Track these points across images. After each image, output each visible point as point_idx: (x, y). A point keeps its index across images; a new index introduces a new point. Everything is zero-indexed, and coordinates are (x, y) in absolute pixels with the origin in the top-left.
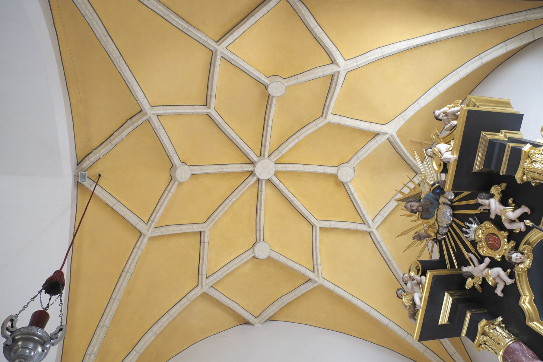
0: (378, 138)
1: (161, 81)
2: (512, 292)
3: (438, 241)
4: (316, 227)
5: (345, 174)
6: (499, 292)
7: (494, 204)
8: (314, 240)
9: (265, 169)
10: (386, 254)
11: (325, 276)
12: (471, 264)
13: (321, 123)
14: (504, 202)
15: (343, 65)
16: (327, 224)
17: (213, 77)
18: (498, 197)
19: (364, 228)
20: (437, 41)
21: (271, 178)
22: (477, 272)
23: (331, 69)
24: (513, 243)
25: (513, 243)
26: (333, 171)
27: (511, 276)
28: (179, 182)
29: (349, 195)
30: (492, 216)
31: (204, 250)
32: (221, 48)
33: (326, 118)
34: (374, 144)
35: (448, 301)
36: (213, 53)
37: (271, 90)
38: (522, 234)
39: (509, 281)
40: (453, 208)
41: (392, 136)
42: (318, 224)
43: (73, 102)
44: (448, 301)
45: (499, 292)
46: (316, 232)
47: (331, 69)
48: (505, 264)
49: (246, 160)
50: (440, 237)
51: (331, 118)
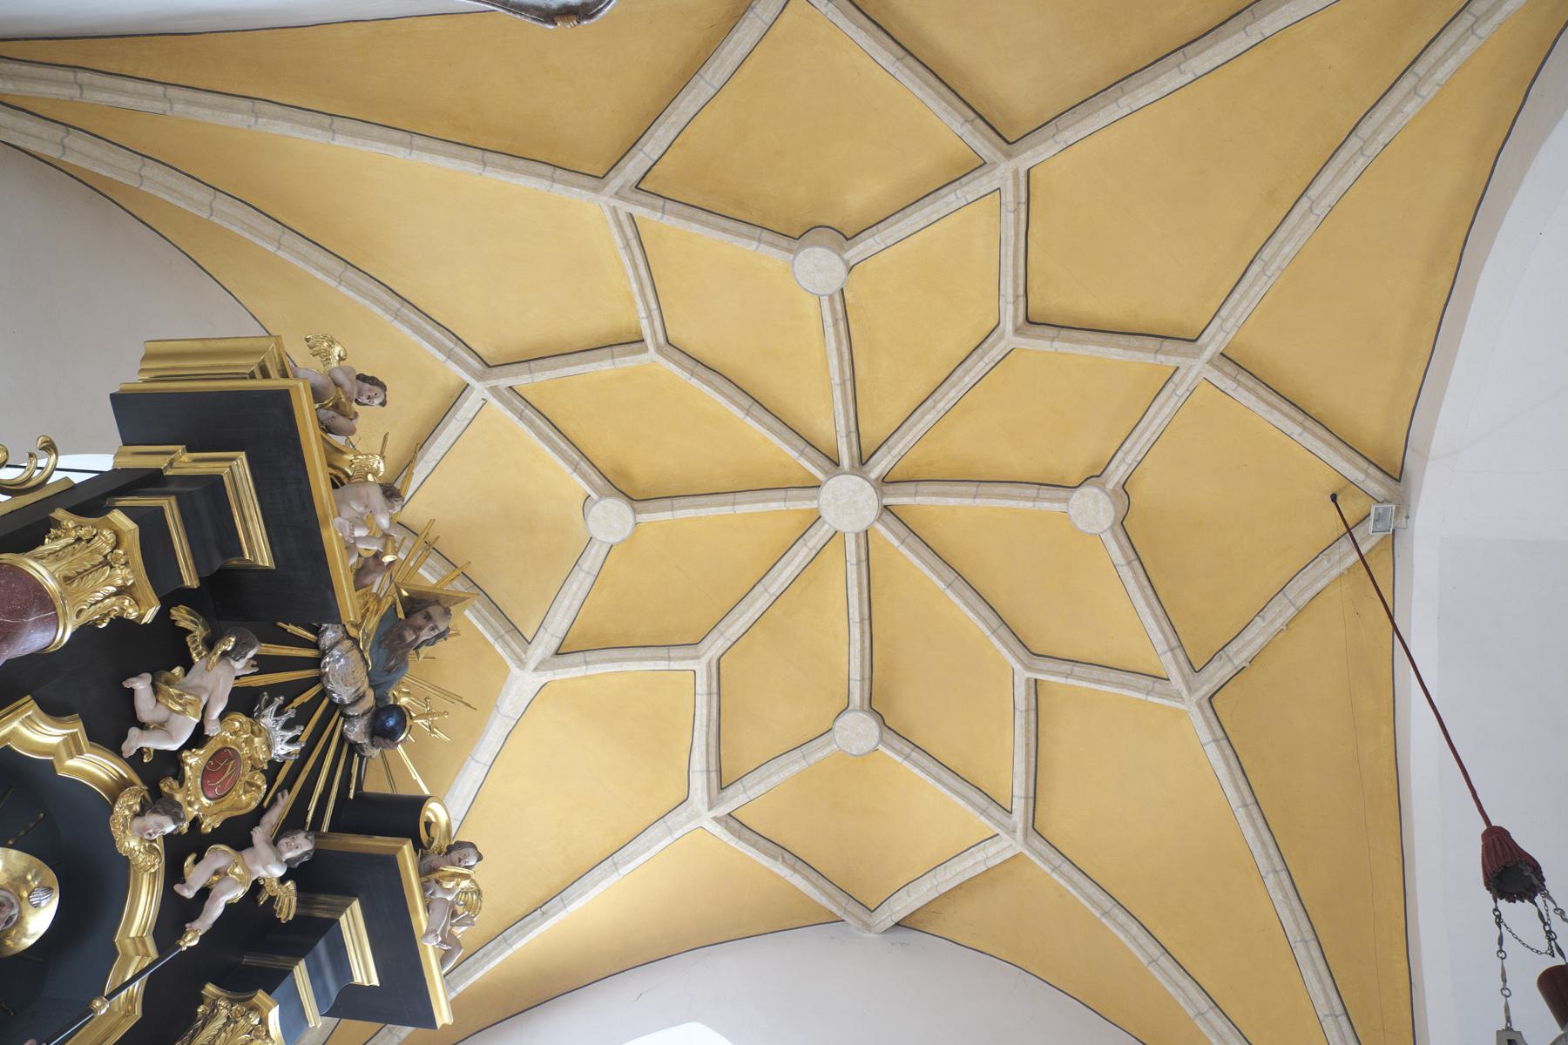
1: (1157, 768)
4: (659, 350)
5: (611, 520)
6: (141, 686)
7: (268, 866)
8: (653, 306)
9: (848, 502)
10: (417, 330)
11: (592, 211)
13: (715, 646)
15: (701, 821)
16: (628, 362)
17: (1027, 762)
18: (272, 888)
21: (862, 709)
28: (1102, 487)
29: (581, 456)
31: (1015, 277)
32: (1008, 846)
34: (558, 624)
35: (258, 550)
36: (1034, 828)
37: (872, 725)
40: (334, 707)
41: (522, 664)
43: (1386, 729)
44: (258, 550)
46: (654, 333)
49: (895, 475)
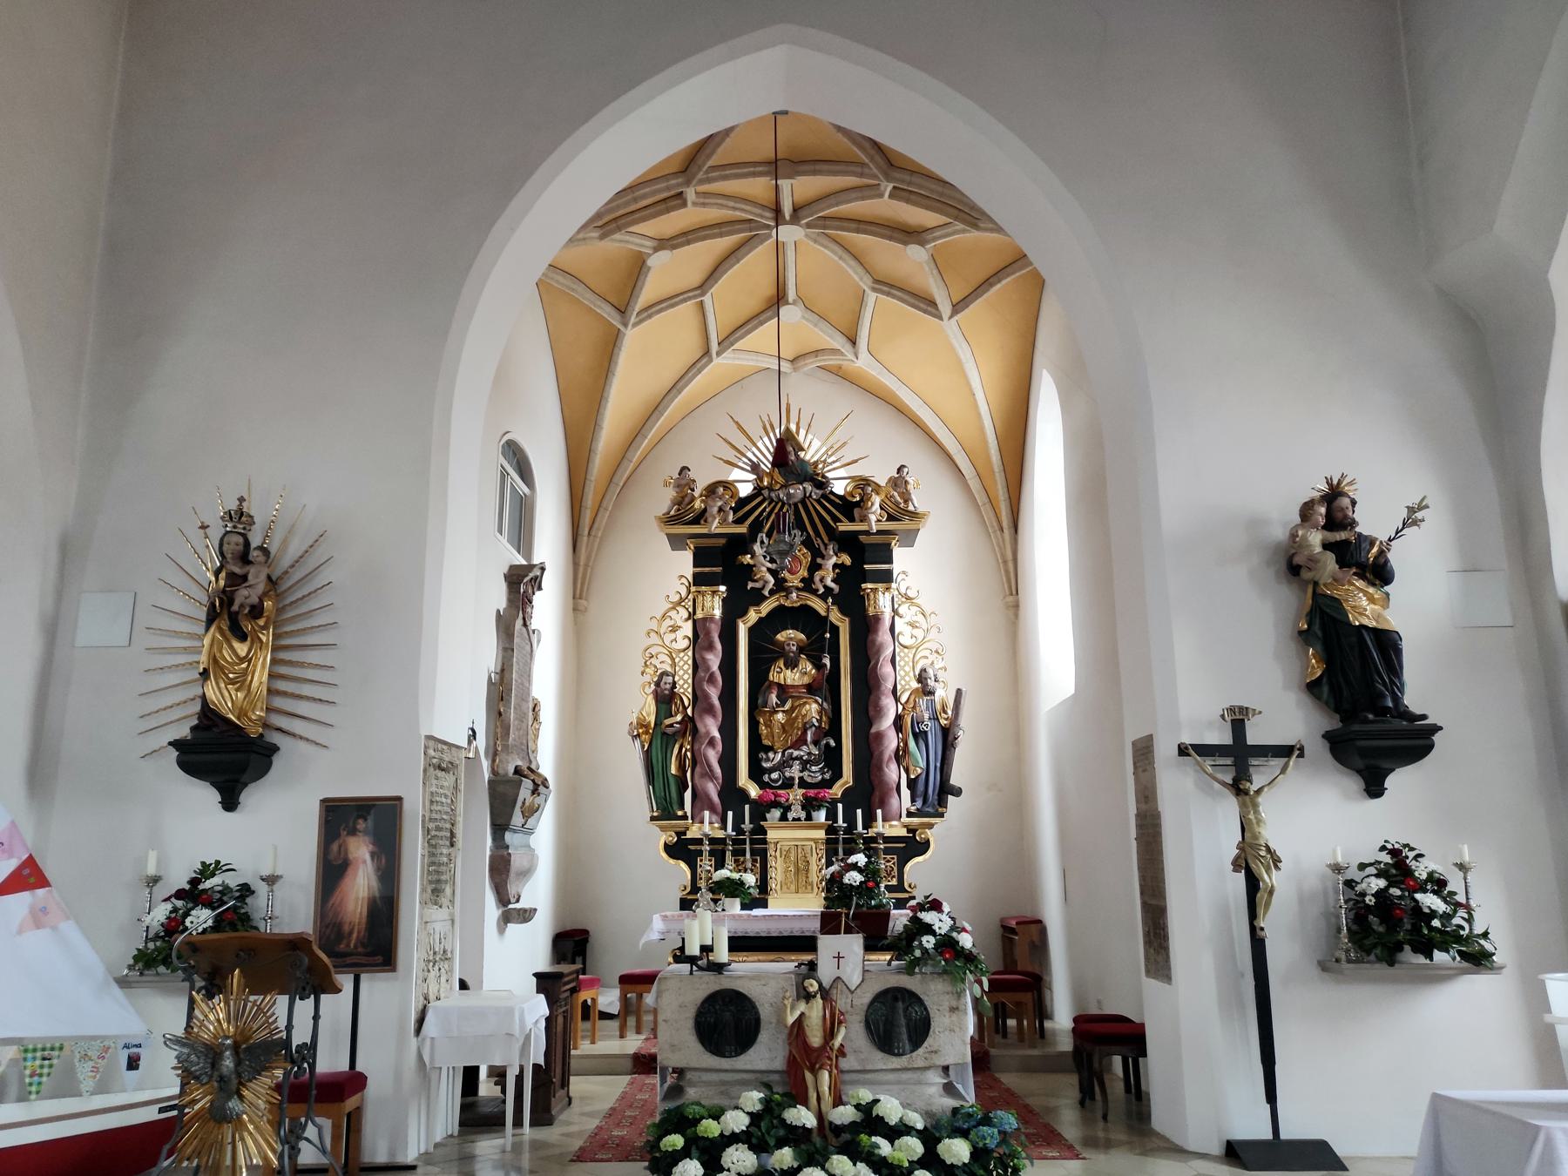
0: (848, 346)
2: (758, 598)
3: (758, 490)
4: (703, 294)
12: (1098, 1096)
14: (835, 566)
19: (714, 347)
20: (979, 415)
22: (758, 556)
23: (945, 308)
24: (801, 585)
25: (801, 585)
26: (791, 295)
27: (772, 592)
30: (819, 560)
33: (874, 290)
38: (814, 592)
39: (766, 593)
40: (803, 501)
42: (707, 299)
45: (750, 585)
47: (945, 308)
48: (781, 586)
50: (766, 493)
51: (872, 297)
